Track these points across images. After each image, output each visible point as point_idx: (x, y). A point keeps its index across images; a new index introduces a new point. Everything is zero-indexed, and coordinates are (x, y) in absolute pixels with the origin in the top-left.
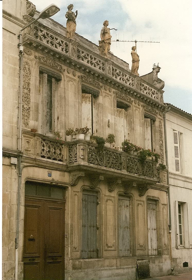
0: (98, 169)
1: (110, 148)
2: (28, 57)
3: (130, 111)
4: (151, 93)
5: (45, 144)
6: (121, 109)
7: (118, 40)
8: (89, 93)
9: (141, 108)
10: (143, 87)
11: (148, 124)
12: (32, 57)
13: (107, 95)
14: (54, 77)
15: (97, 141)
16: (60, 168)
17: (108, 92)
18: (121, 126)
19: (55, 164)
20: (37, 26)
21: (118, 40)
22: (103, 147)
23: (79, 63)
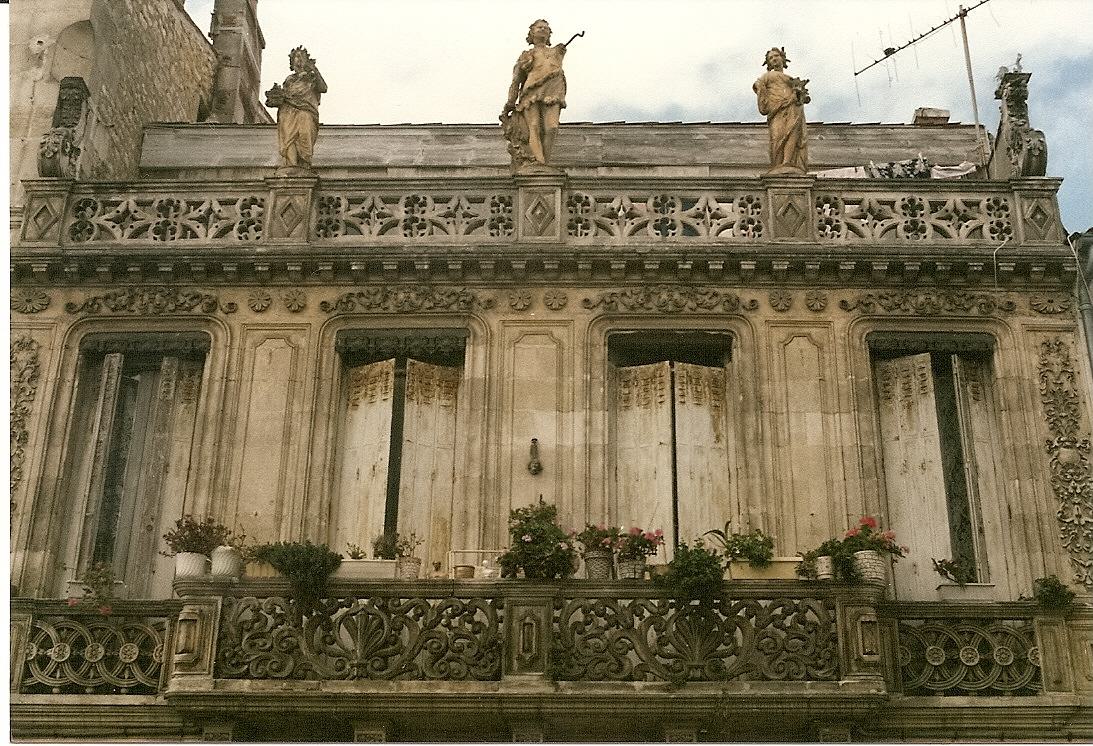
0: (295, 698)
1: (396, 583)
2: (31, 318)
3: (475, 363)
4: (804, 204)
5: (989, 637)
6: (652, 367)
7: (889, 52)
8: (380, 356)
9: (839, 321)
10: (133, 207)
11: (915, 383)
12: (56, 312)
13: (530, 329)
14: (170, 353)
15: (281, 566)
16: (146, 721)
17: (800, 313)
18: (655, 444)
19: (102, 709)
20: (91, 197)
21: (889, 52)
22: (721, 584)
23: (173, 255)
